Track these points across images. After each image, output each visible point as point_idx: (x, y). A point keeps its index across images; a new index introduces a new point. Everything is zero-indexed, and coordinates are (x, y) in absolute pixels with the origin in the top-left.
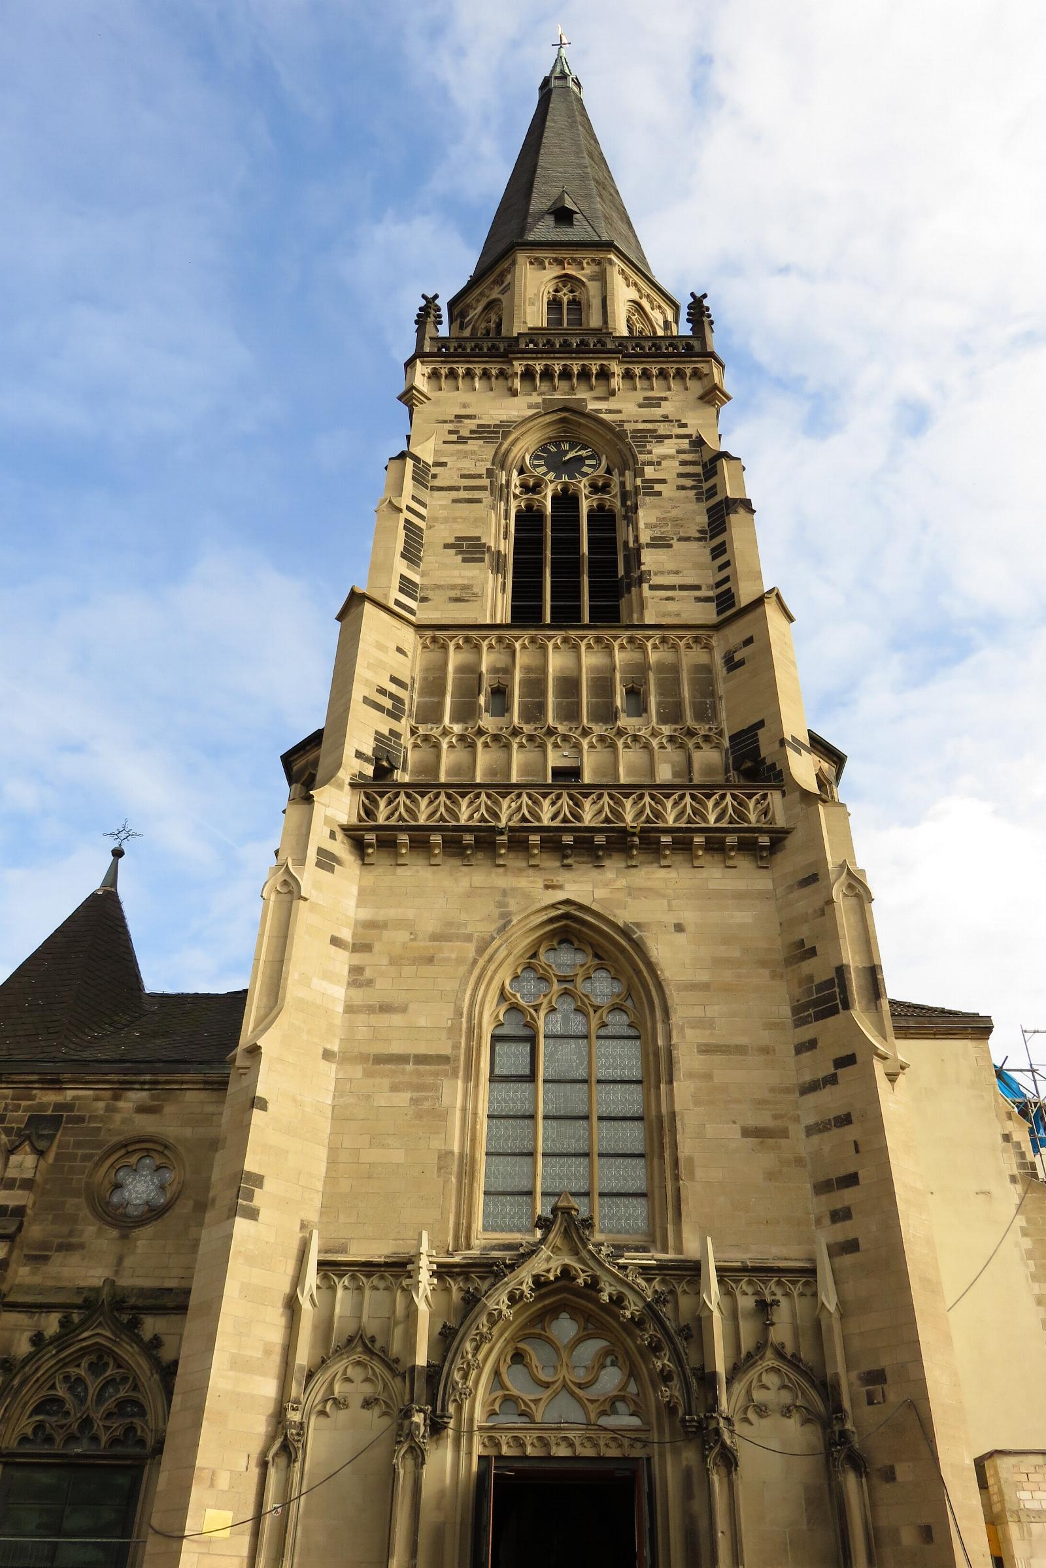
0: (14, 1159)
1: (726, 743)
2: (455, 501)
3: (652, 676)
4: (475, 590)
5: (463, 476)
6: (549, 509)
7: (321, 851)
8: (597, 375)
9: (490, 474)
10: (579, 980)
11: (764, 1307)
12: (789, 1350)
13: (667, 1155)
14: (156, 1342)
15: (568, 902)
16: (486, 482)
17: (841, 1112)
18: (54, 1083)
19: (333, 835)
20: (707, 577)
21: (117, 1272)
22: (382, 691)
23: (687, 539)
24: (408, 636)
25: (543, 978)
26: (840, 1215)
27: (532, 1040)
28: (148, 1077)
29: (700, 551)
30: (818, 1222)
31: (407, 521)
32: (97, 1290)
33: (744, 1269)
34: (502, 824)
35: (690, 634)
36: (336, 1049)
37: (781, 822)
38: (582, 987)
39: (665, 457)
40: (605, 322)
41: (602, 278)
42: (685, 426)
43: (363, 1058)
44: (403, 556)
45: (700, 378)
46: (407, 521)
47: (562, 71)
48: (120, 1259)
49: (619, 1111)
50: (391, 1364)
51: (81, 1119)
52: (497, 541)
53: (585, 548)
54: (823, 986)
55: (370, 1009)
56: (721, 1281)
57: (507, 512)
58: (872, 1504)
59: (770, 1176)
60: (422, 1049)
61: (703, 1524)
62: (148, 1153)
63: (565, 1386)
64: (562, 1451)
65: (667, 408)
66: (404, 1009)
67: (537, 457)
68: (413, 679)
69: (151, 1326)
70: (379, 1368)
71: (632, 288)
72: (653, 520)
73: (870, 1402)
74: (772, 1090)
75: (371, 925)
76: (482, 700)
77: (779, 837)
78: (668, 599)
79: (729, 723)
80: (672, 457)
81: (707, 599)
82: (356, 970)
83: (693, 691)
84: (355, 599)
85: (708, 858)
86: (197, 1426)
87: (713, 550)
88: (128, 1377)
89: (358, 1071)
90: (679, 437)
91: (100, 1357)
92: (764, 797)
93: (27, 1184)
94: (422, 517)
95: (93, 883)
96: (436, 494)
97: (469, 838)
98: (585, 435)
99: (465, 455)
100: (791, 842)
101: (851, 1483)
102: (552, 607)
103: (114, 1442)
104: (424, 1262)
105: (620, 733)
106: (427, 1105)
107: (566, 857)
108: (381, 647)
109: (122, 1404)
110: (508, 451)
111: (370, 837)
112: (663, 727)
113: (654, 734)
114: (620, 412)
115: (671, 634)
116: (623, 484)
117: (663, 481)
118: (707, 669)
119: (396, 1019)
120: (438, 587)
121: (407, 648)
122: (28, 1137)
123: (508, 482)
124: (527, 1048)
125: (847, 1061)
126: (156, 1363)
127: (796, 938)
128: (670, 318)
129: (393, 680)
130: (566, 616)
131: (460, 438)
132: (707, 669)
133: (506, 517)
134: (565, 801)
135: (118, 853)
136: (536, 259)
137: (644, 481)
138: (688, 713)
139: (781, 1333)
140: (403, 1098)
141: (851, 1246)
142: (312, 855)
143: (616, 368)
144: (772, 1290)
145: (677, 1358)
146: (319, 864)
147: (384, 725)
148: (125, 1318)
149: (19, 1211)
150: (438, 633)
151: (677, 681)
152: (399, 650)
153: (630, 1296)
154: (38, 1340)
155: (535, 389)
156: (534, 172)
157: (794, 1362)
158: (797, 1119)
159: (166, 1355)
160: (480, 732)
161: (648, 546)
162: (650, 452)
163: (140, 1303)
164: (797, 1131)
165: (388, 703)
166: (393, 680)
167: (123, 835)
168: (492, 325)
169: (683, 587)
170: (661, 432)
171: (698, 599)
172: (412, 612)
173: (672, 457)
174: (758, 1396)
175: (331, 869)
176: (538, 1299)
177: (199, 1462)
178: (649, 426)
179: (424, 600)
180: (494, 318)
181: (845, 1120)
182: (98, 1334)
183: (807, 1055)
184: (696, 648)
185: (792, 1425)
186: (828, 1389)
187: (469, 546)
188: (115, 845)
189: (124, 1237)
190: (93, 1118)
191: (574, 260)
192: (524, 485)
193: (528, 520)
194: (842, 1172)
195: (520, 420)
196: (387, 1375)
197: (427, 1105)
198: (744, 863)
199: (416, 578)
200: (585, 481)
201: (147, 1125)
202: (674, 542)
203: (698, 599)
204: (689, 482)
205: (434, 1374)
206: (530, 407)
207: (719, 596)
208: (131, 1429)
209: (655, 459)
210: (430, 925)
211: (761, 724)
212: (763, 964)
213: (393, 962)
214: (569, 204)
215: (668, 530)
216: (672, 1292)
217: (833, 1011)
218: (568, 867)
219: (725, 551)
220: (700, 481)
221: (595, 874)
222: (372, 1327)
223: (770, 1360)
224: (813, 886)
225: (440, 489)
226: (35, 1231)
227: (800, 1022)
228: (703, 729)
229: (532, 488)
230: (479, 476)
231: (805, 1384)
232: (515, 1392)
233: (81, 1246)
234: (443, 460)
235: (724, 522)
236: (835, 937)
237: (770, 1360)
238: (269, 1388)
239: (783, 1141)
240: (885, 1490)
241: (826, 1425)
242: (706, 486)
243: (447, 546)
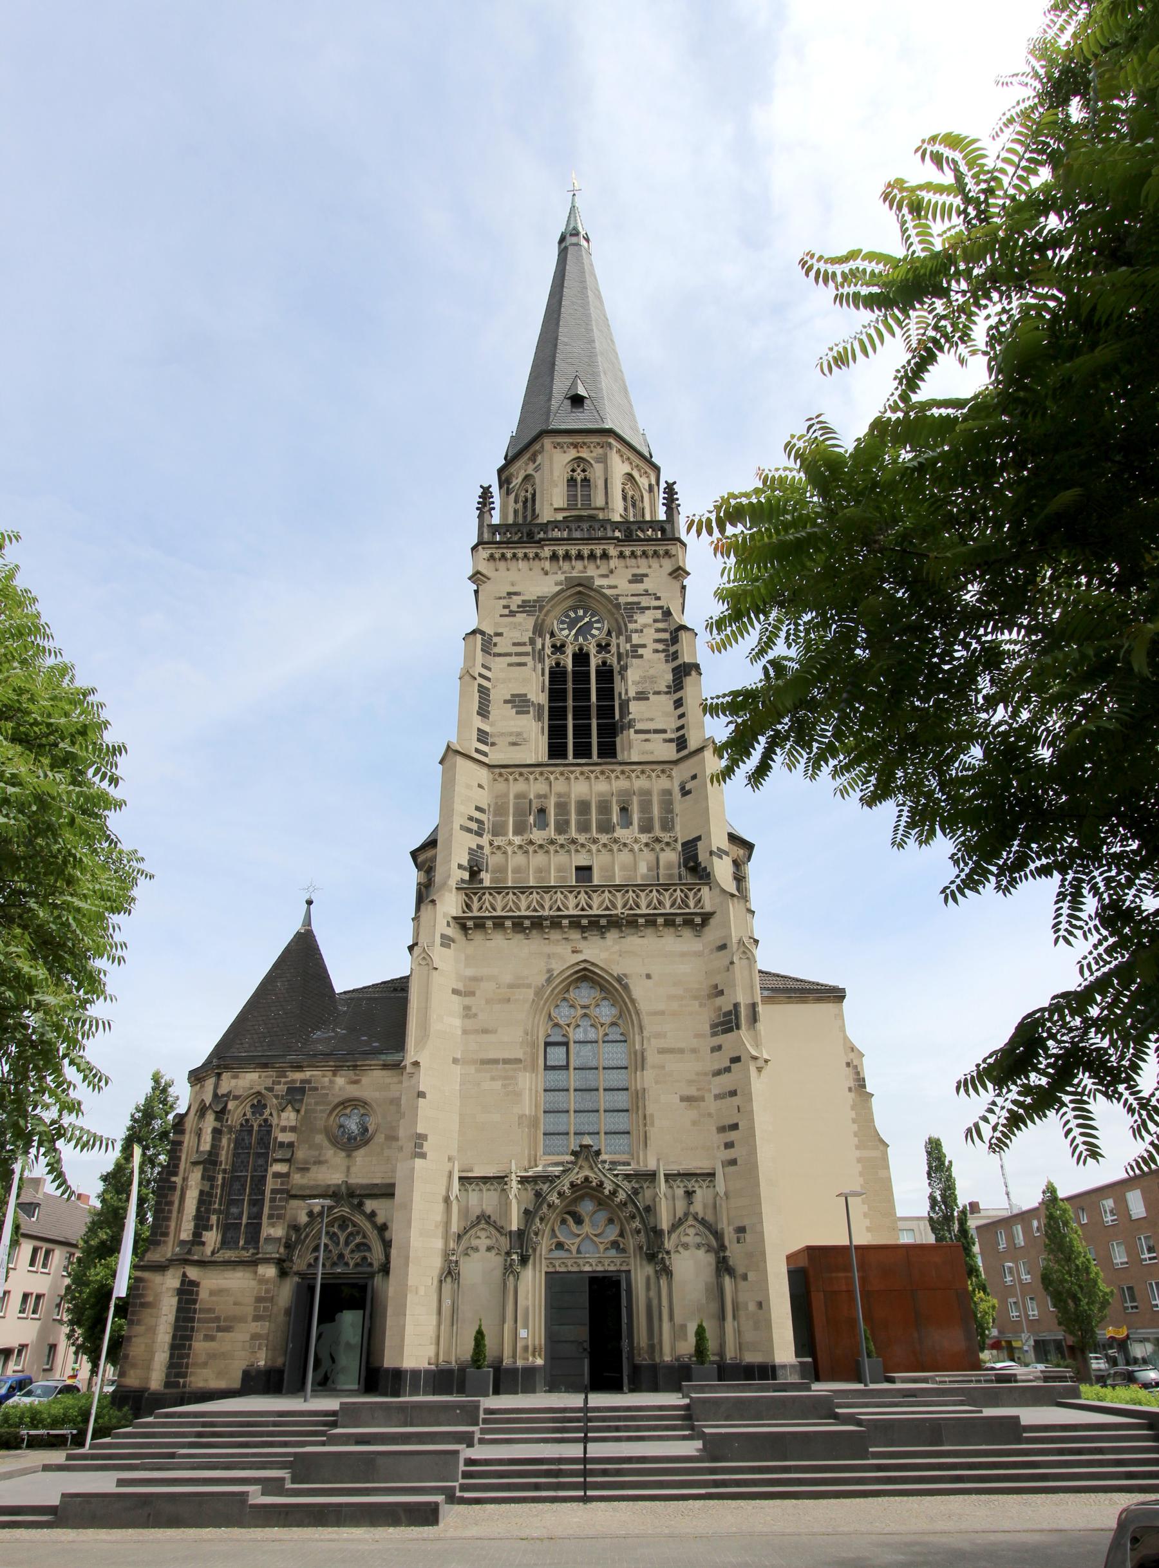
0: (284, 1115)
1: (680, 848)
2: (510, 665)
3: (635, 799)
4: (525, 736)
5: (515, 644)
6: (570, 667)
7: (443, 936)
8: (601, 558)
9: (532, 642)
10: (592, 1007)
11: (689, 1194)
12: (700, 1216)
13: (640, 1112)
14: (373, 1214)
15: (585, 961)
16: (529, 649)
17: (732, 1089)
18: (299, 1068)
19: (448, 925)
20: (671, 723)
21: (347, 1176)
22: (471, 819)
23: (658, 693)
24: (483, 775)
25: (572, 1006)
27: (566, 1044)
29: (667, 702)
30: (718, 1147)
31: (480, 685)
32: (338, 1186)
33: (679, 1175)
34: (546, 913)
35: (659, 767)
36: (459, 1056)
37: (708, 908)
38: (594, 1012)
39: (645, 626)
40: (607, 503)
41: (604, 460)
42: (658, 598)
43: (474, 1062)
44: (478, 713)
45: (670, 557)
46: (480, 685)
47: (575, 229)
48: (348, 1168)
49: (615, 1085)
50: (500, 1230)
51: (316, 1089)
52: (537, 695)
53: (594, 723)
55: (476, 1032)
56: (666, 1181)
57: (543, 670)
58: (736, 1291)
59: (694, 1123)
60: (507, 1056)
61: (655, 1302)
62: (355, 1107)
63: (587, 1235)
65: (648, 584)
66: (495, 1032)
67: (563, 622)
68: (489, 805)
69: (370, 1205)
70: (493, 1231)
71: (627, 463)
72: (637, 679)
73: (738, 1242)
74: (698, 1074)
75: (476, 979)
76: (531, 819)
77: (706, 917)
78: (646, 740)
79: (682, 834)
80: (650, 626)
81: (671, 741)
82: (467, 1008)
83: (661, 808)
84: (450, 750)
85: (666, 930)
86: (407, 1265)
87: (675, 702)
88: (359, 1231)
89: (472, 1069)
90: (656, 608)
91: (344, 1222)
92: (699, 890)
93: (293, 1129)
94: (488, 679)
95: (296, 926)
96: (497, 659)
97: (527, 923)
99: (515, 626)
100: (713, 921)
101: (727, 1280)
102: (574, 726)
103: (357, 1265)
104: (513, 1176)
105: (616, 841)
106: (510, 1088)
107: (583, 932)
108: (469, 787)
109: (358, 1246)
110: (544, 620)
111: (470, 924)
112: (641, 836)
113: (636, 841)
114: (615, 587)
115: (647, 768)
116: (618, 646)
117: (644, 646)
118: (668, 792)
119: (491, 1038)
120: (502, 734)
121: (485, 783)
122: (290, 1102)
123: (543, 645)
124: (565, 1049)
125: (736, 1060)
126: (374, 1224)
127: (714, 983)
128: (653, 482)
129: (478, 809)
130: (583, 751)
131: (511, 611)
132: (668, 792)
133: (543, 675)
134: (583, 896)
135: (310, 903)
136: (558, 444)
137: (632, 646)
138: (657, 825)
139: (698, 1207)
140: (498, 1085)
141: (733, 1162)
142: (438, 940)
143: (613, 551)
144: (691, 1184)
145: (643, 1221)
146: (442, 945)
147: (472, 841)
148: (356, 1201)
149: (291, 1145)
150: (503, 770)
151: (650, 802)
152: (480, 786)
153: (621, 1191)
154: (310, 1214)
155: (560, 568)
156: (556, 345)
157: (703, 1222)
158: (710, 1090)
159: (380, 1220)
160: (531, 843)
161: (636, 699)
162: (636, 622)
163: (363, 1192)
164: (709, 1098)
165: (474, 826)
166: (478, 809)
167: (311, 889)
168: (529, 496)
169: (656, 731)
170: (643, 604)
171: (666, 741)
172: (485, 754)
173: (650, 626)
174: (685, 1239)
175: (449, 946)
176: (572, 1193)
177: (410, 1283)
178: (635, 599)
179: (493, 744)
180: (530, 490)
181: (733, 1093)
182: (345, 1210)
184: (663, 777)
185: (701, 1253)
186: (718, 1235)
187: (520, 701)
188: (307, 897)
189: (349, 1156)
190: (323, 1088)
191: (584, 443)
192: (554, 646)
193: (557, 676)
194: (731, 1122)
195: (550, 595)
196: (498, 1235)
197: (510, 1088)
198: (687, 933)
199: (487, 728)
200: (593, 642)
201: (353, 1091)
202: (650, 696)
203: (666, 741)
204: (661, 647)
205: (521, 1233)
206: (556, 584)
207: (678, 738)
208: (364, 1258)
209: (639, 628)
210: (507, 978)
211: (699, 838)
212: (696, 998)
213: (488, 1001)
214: (582, 391)
215: (647, 687)
216: (641, 1187)
217: (730, 1030)
218: (585, 938)
219: (681, 705)
220: (668, 645)
221: (600, 942)
222: (489, 1211)
223: (691, 1221)
225: (500, 655)
226: (300, 1154)
227: (714, 1034)
228: (666, 836)
229: (559, 648)
230: (524, 644)
231: (708, 1233)
232: (562, 1239)
233: (326, 1162)
234: (500, 631)
235: (682, 682)
236: (733, 986)
237: (691, 1221)
238: (439, 1244)
239: (702, 1104)
240: (742, 1284)
241: (717, 1253)
242: (672, 649)
243: (506, 702)
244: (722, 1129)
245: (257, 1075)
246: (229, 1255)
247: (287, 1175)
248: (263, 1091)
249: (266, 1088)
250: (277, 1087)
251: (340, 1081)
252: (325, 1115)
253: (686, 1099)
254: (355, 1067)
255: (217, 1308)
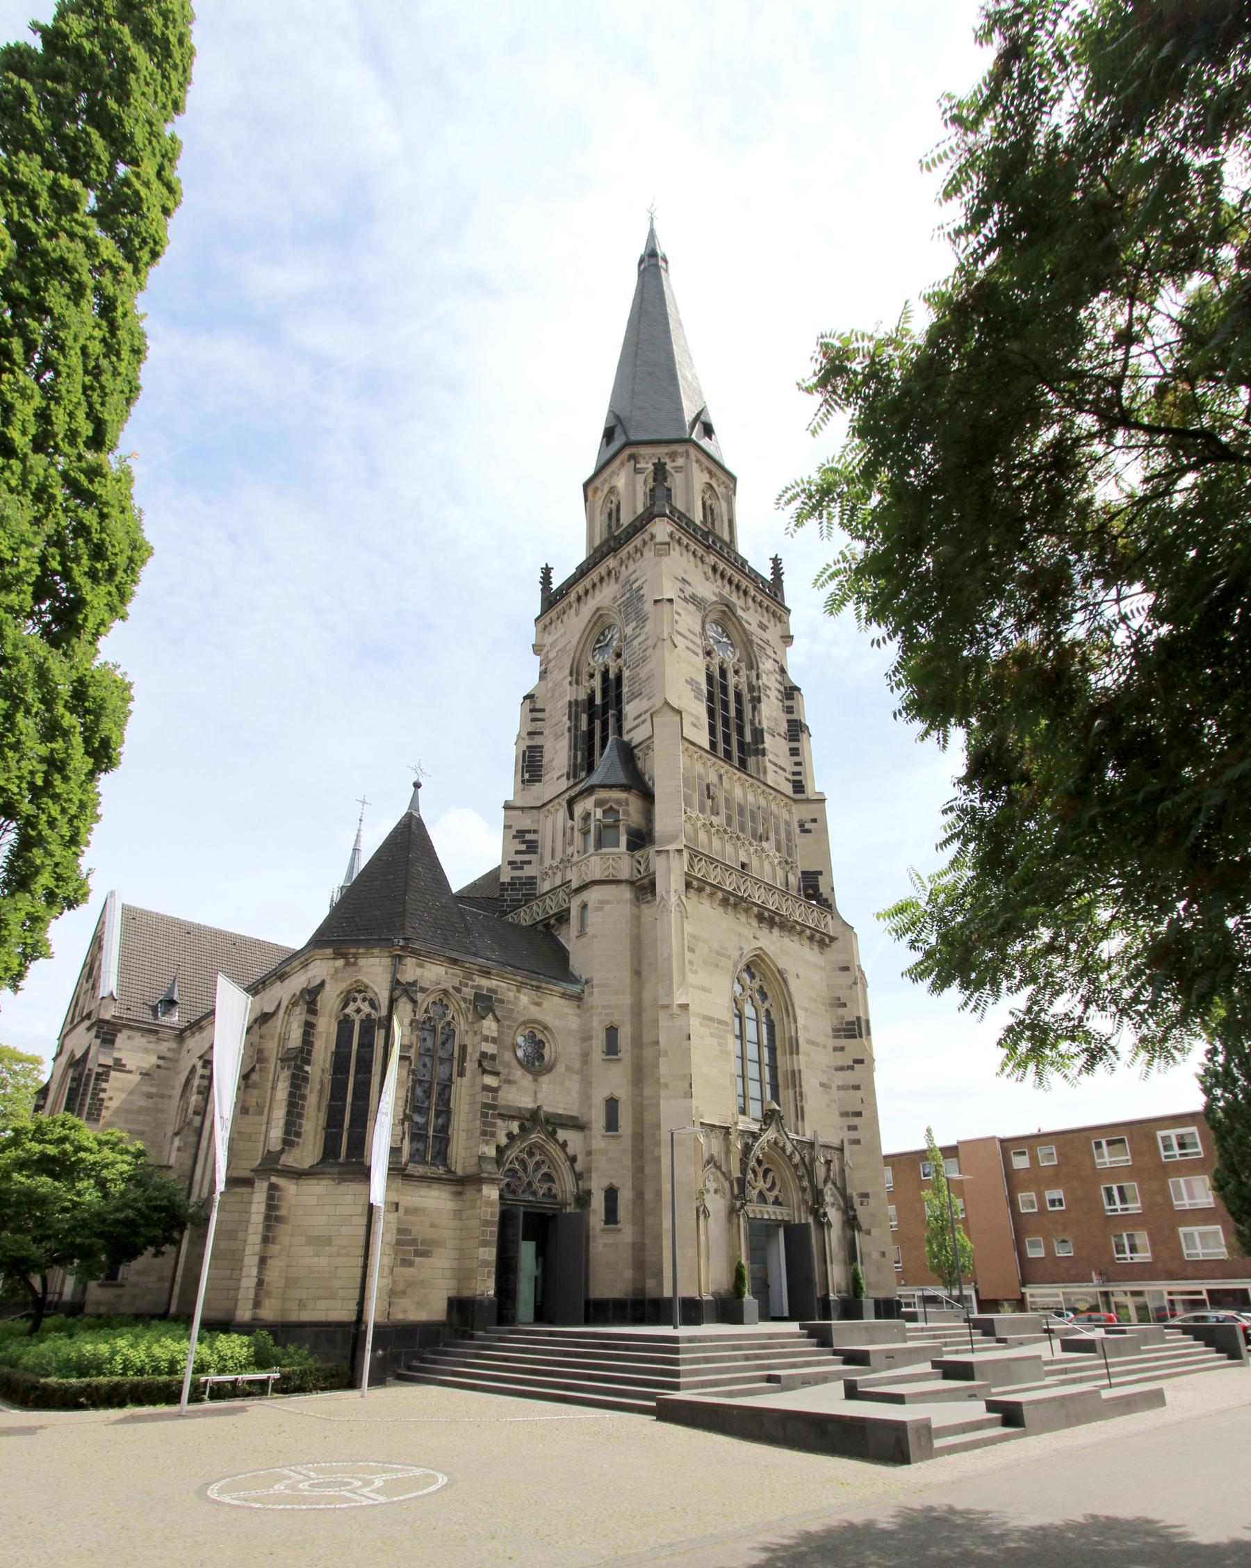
15: (760, 949)
26: (852, 1128)
28: (535, 983)
48: (536, 1093)
54: (848, 1023)
64: (766, 1217)
69: (562, 1134)
88: (553, 1163)
93: (494, 1041)
98: (731, 628)
111: (695, 883)
135: (417, 785)
154: (510, 1136)
181: (857, 1088)
183: (839, 1053)
188: (415, 780)
189: (535, 1080)
190: (509, 1002)
217: (854, 1037)
224: (846, 973)
244: (845, 1114)
245: (443, 969)
246: (420, 1170)
247: (495, 1090)
248: (451, 990)
249: (454, 988)
250: (464, 989)
251: (524, 999)
252: (512, 1032)
253: (823, 1085)
254: (538, 988)
255: (414, 1229)
